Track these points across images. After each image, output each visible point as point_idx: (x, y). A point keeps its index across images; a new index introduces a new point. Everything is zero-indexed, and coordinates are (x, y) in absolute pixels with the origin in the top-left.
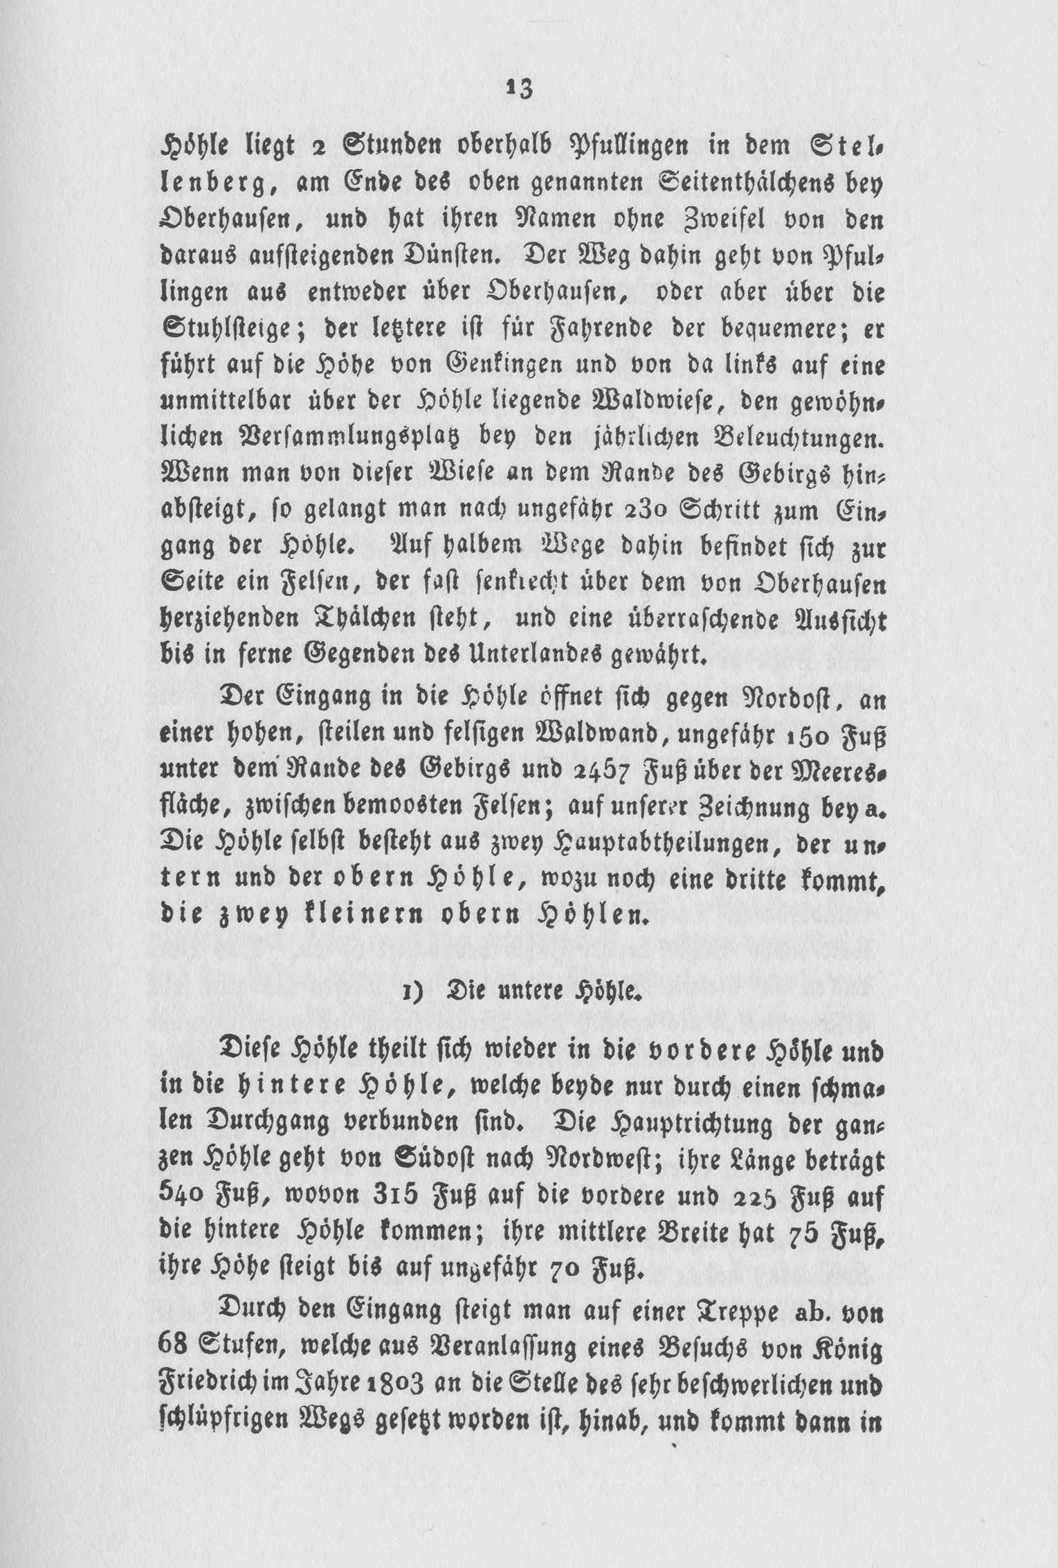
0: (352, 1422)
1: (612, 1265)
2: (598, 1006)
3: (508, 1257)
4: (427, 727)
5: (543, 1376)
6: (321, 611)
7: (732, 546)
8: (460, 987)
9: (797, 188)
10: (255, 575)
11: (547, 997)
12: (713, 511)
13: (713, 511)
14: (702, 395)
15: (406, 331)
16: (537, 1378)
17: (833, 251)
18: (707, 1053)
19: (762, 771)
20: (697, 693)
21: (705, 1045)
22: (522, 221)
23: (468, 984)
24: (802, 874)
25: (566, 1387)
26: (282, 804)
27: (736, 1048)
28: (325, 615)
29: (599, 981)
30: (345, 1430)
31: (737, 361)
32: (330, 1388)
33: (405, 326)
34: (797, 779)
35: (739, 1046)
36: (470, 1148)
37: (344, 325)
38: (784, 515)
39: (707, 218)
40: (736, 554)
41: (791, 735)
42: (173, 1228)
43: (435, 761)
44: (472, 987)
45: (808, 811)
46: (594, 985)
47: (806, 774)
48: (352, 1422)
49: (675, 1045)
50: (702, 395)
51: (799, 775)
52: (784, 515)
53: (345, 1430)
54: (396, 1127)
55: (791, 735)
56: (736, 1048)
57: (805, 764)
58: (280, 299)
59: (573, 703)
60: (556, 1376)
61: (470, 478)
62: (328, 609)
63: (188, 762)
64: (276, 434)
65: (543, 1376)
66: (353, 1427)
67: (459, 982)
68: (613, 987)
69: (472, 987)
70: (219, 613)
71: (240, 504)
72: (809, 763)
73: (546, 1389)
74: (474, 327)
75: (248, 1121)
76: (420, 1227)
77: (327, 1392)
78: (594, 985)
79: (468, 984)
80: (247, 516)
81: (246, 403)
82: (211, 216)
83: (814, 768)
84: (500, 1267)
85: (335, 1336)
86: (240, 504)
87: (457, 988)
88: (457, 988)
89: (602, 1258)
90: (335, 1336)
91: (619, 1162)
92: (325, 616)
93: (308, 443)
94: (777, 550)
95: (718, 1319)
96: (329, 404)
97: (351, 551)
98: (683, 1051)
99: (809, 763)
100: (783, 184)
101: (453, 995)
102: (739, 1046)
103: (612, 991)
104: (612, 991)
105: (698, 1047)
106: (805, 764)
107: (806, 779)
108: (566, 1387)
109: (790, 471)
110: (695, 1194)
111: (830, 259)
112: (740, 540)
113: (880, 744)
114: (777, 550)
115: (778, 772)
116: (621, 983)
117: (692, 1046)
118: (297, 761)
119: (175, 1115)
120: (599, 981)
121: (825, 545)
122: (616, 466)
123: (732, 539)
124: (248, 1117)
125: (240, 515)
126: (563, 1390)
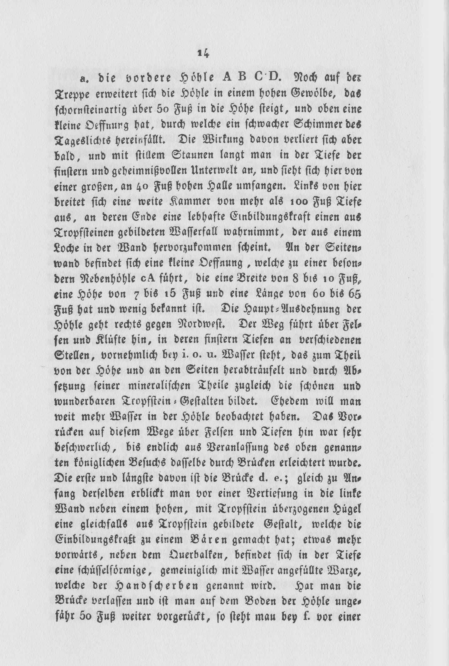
4: (112, 307)
5: (69, 353)
16: (67, 354)
18: (150, 79)
20: (158, 322)
21: (149, 76)
22: (297, 79)
27: (162, 76)
35: (163, 76)
37: (355, 76)
38: (187, 249)
41: (166, 293)
43: (270, 521)
49: (137, 76)
52: (187, 249)
54: (64, 404)
55: (166, 293)
56: (162, 76)
58: (330, 420)
61: (121, 434)
63: (182, 306)
64: (199, 231)
65: (69, 353)
71: (281, 106)
80: (284, 111)
81: (104, 494)
82: (191, 554)
85: (269, 259)
86: (281, 106)
90: (269, 259)
93: (244, 188)
96: (325, 94)
97: (359, 465)
98: (140, 78)
102: (163, 76)
105: (146, 76)
109: (139, 384)
117: (144, 76)
125: (281, 111)
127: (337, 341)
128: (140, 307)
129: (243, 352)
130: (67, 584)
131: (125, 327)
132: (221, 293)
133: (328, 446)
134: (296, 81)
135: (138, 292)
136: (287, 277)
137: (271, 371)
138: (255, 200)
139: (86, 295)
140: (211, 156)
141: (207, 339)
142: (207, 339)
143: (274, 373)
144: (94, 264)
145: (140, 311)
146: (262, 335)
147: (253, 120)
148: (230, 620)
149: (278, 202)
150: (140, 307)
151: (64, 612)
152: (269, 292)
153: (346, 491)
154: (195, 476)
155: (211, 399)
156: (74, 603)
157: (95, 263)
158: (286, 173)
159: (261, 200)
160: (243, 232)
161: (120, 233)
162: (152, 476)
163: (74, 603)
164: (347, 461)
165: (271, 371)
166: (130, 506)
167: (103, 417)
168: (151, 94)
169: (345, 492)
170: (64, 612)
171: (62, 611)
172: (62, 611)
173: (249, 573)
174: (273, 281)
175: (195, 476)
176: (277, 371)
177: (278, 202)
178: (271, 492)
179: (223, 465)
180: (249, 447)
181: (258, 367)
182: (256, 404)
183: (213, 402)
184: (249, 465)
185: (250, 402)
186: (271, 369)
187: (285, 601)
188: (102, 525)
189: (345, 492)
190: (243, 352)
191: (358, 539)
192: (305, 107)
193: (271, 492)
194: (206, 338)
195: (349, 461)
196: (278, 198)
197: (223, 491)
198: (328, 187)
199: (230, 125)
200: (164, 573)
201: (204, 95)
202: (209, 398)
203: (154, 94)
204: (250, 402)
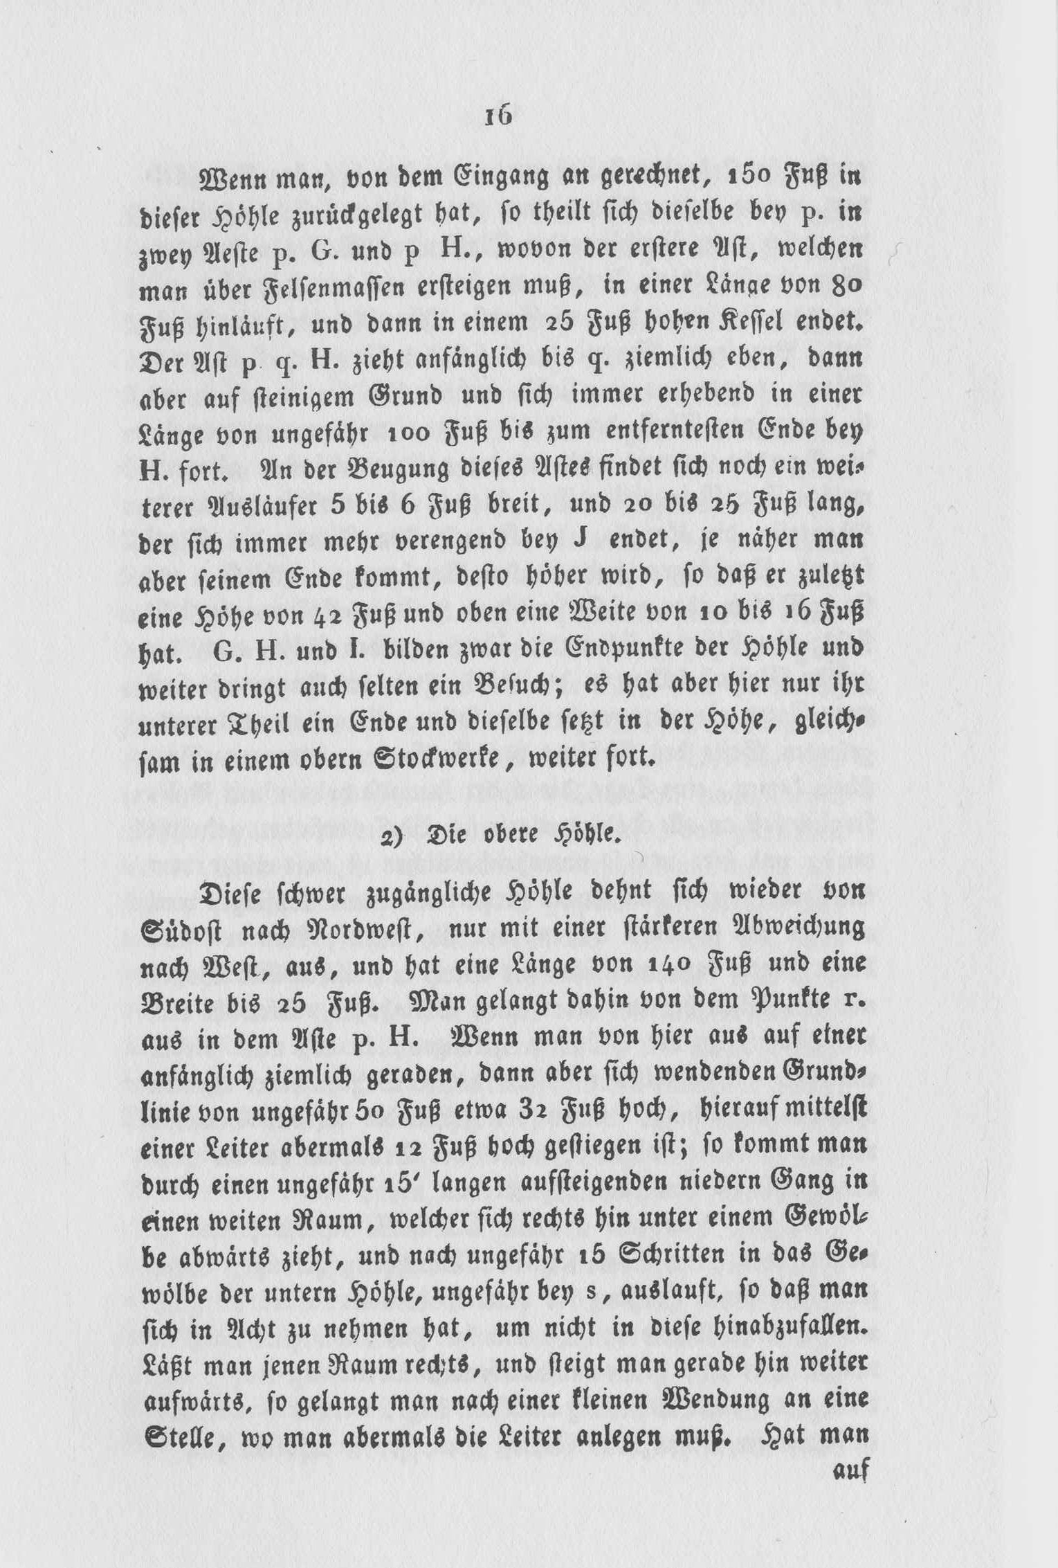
2: (579, 848)
3: (535, 1245)
6: (234, 719)
7: (606, 466)
8: (440, 832)
9: (837, 253)
10: (843, 1392)
11: (523, 840)
12: (471, 893)
13: (471, 893)
14: (250, 890)
17: (761, 993)
19: (781, 889)
22: (314, 933)
23: (448, 829)
28: (238, 723)
29: (578, 824)
31: (153, 1110)
34: (415, 1010)
40: (610, 474)
42: (665, 210)
44: (452, 831)
45: (814, 656)
46: (573, 828)
47: (424, 1005)
50: (250, 890)
51: (417, 1005)
57: (423, 994)
62: (241, 717)
67: (440, 827)
68: (592, 830)
69: (452, 831)
72: (427, 993)
75: (173, 1187)
78: (573, 828)
79: (448, 829)
83: (432, 998)
84: (527, 1255)
85: (423, 1210)
87: (436, 834)
88: (436, 834)
90: (423, 1210)
91: (668, 1074)
92: (239, 724)
94: (652, 469)
99: (427, 993)
100: (823, 249)
101: (433, 841)
103: (590, 833)
104: (590, 833)
106: (423, 994)
107: (424, 1009)
110: (786, 959)
111: (758, 1000)
112: (614, 460)
114: (652, 469)
115: (764, 684)
116: (600, 825)
118: (303, 1214)
123: (606, 459)
124: (173, 1183)
128: (305, 394)
131: (547, 1226)
132: (605, 503)
133: (485, 999)
134: (313, 938)
136: (184, 288)
137: (292, 509)
143: (302, 513)
145: (306, 404)
146: (648, 419)
148: (277, 897)
149: (371, 1150)
150: (305, 394)
151: (350, 1177)
152: (193, 1074)
154: (664, 1141)
155: (389, 682)
158: (684, 897)
159: (363, 431)
161: (481, 1003)
162: (255, 250)
165: (292, 509)
170: (350, 1177)
174: (643, 1005)
175: (664, 1141)
176: (376, 689)
177: (371, 1150)
180: (374, 288)
182: (652, 762)
183: (393, 689)
184: (810, 1077)
185: (845, 323)
186: (292, 503)
188: (525, 1146)
191: (558, 1252)
192: (624, 1179)
196: (372, 1141)
199: (465, 968)
200: (309, 440)
201: (268, 220)
204: (845, 323)
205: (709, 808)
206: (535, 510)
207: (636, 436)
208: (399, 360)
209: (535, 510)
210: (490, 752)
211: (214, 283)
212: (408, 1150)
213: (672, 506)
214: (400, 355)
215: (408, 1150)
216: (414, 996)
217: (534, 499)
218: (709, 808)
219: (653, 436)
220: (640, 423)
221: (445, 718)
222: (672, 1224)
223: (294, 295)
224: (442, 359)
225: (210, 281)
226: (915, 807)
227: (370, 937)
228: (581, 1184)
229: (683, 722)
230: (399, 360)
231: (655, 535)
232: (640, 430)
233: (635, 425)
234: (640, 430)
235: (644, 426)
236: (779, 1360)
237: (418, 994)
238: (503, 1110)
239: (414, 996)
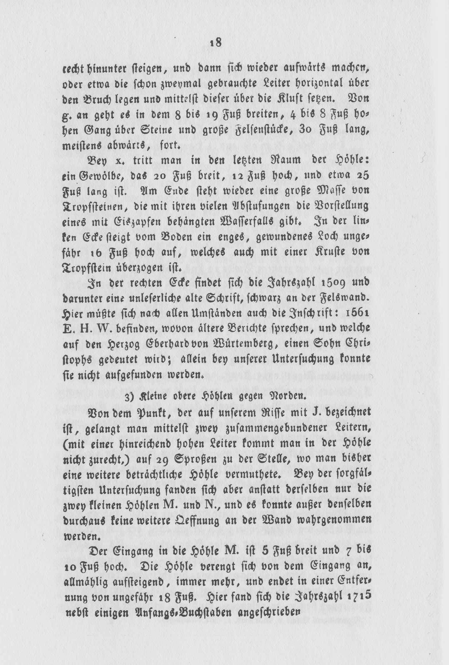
0: (169, 614)
1: (117, 251)
15: (248, 162)
16: (269, 457)
24: (111, 518)
25: (282, 460)
26: (233, 298)
29: (212, 392)
30: (167, 617)
32: (145, 600)
33: (247, 160)
34: (320, 193)
36: (86, 608)
39: (302, 67)
47: (323, 191)
48: (169, 614)
51: (320, 192)
53: (167, 617)
57: (323, 187)
59: (198, 524)
60: (278, 456)
66: (170, 616)
70: (283, 610)
72: (324, 186)
73: (274, 461)
74: (228, 460)
76: (186, 580)
77: (144, 601)
85: (215, 202)
89: (113, 249)
92: (68, 206)
95: (72, 210)
99: (324, 186)
106: (323, 187)
107: (323, 193)
108: (282, 460)
113: (96, 569)
119: (152, 504)
120: (212, 392)
121: (351, 66)
122: (277, 157)
126: (281, 461)
127: (187, 375)
129: (241, 218)
130: (94, 427)
132: (188, 68)
135: (350, 548)
138: (179, 220)
139: (351, 443)
140: (75, 131)
141: (198, 283)
142: (198, 283)
144: (126, 330)
147: (268, 608)
153: (360, 218)
156: (351, 357)
157: (126, 329)
160: (181, 206)
163: (351, 357)
164: (185, 373)
166: (103, 610)
167: (78, 254)
168: (130, 314)
169: (358, 219)
171: (68, 249)
172: (68, 249)
173: (220, 346)
178: (69, 489)
179: (77, 524)
181: (145, 472)
187: (115, 414)
189: (358, 219)
190: (241, 218)
193: (69, 489)
194: (196, 281)
195: (187, 372)
197: (316, 578)
198: (197, 345)
202: (207, 326)
203: (133, 314)
205: (324, 386)
206: (218, 178)
207: (353, 583)
208: (215, 191)
209: (218, 178)
210: (67, 236)
211: (238, 95)
212: (238, 177)
213: (360, 551)
214: (215, 189)
215: (238, 177)
216: (319, 188)
217: (218, 174)
218: (324, 386)
219: (361, 583)
220: (355, 577)
221: (364, 280)
222: (286, 507)
223: (248, 132)
224: (230, 413)
225: (237, 94)
226: (394, 386)
227: (120, 148)
228: (142, 69)
229: (332, 444)
230: (215, 191)
231: (267, 472)
232: (355, 580)
233: (353, 578)
234: (355, 580)
235: (357, 578)
236: (124, 520)
237: (320, 187)
238: (108, 84)
239: (319, 188)
